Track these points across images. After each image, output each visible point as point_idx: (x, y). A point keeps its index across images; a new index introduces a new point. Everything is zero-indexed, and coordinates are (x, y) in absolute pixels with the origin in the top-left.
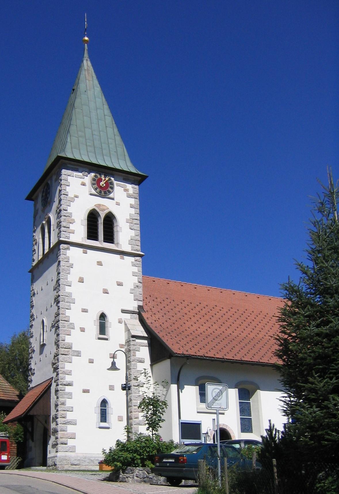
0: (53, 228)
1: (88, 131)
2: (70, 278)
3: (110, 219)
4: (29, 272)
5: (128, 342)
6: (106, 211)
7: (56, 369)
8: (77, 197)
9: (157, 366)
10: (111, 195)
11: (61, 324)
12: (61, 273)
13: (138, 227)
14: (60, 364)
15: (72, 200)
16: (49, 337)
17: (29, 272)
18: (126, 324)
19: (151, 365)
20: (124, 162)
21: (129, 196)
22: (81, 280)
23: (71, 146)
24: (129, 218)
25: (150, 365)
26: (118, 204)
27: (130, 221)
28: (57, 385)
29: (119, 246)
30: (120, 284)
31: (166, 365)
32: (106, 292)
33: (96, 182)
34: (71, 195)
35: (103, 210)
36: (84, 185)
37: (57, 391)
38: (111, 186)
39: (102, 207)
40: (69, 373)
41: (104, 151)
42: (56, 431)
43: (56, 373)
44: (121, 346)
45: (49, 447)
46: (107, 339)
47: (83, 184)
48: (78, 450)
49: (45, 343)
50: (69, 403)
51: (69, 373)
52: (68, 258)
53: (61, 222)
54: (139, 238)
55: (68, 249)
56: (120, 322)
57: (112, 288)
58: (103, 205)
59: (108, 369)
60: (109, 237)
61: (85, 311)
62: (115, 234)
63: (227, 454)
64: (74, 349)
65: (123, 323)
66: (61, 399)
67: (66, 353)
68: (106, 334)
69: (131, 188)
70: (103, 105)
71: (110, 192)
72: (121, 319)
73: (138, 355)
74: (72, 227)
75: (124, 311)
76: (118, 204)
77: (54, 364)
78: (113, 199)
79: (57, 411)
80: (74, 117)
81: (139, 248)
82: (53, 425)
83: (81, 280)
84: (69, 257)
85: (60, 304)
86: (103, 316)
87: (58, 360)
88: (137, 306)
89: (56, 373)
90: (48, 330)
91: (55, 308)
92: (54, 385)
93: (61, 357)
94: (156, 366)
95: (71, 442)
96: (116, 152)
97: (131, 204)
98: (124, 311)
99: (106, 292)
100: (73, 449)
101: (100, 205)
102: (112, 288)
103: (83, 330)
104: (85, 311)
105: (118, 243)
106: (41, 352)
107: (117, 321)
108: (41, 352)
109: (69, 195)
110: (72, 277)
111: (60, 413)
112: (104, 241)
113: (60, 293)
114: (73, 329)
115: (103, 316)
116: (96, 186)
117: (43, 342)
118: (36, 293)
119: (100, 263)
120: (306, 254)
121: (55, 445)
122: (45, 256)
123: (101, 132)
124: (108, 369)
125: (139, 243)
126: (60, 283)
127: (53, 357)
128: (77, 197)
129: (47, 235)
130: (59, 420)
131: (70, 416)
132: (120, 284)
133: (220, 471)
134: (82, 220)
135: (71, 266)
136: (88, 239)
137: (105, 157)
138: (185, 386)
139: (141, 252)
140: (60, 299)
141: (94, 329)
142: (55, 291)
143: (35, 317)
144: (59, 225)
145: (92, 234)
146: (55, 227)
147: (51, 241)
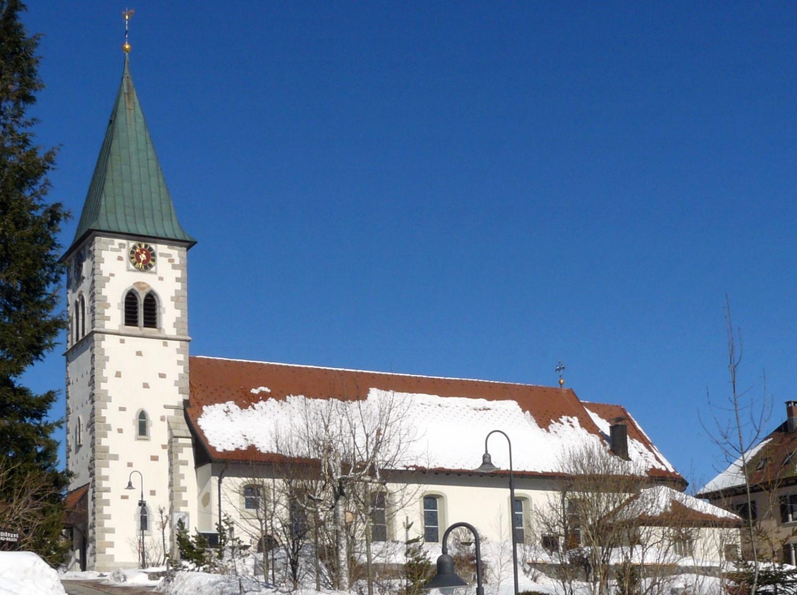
0: (88, 310)
1: (127, 185)
2: (105, 373)
3: (151, 301)
4: (64, 355)
5: (170, 442)
6: (147, 291)
7: (92, 474)
8: (112, 275)
10: (153, 269)
11: (96, 425)
13: (185, 305)
14: (96, 470)
16: (85, 437)
17: (64, 355)
18: (168, 423)
20: (170, 222)
21: (174, 267)
22: (118, 375)
25: (195, 468)
26: (161, 279)
27: (176, 299)
29: (162, 331)
30: (162, 376)
31: (208, 467)
32: (146, 386)
33: (134, 255)
34: (105, 274)
35: (143, 289)
36: (120, 260)
37: (93, 498)
38: (153, 258)
40: (106, 478)
41: (146, 212)
42: (93, 540)
43: (92, 478)
44: (164, 447)
45: (88, 556)
47: (120, 258)
49: (81, 443)
51: (106, 478)
52: (103, 350)
55: (103, 339)
56: (162, 419)
57: (154, 381)
58: (144, 283)
59: (126, 489)
60: (151, 320)
61: (122, 409)
62: (158, 316)
63: (348, 560)
64: (111, 452)
65: (166, 421)
66: (97, 507)
67: (102, 458)
70: (147, 143)
71: (151, 266)
73: (181, 457)
75: (165, 407)
76: (161, 279)
77: (90, 469)
78: (155, 273)
79: (94, 519)
80: (109, 168)
81: (186, 331)
82: (90, 532)
83: (118, 375)
85: (96, 403)
86: (142, 415)
87: (94, 465)
88: (181, 400)
89: (92, 478)
90: (84, 429)
93: (97, 462)
96: (161, 211)
99: (146, 386)
100: (112, 557)
101: (139, 283)
102: (154, 381)
103: (120, 431)
104: (122, 409)
105: (160, 328)
106: (77, 452)
108: (77, 452)
110: (108, 371)
111: (98, 520)
112: (145, 326)
114: (110, 430)
115: (142, 415)
117: (79, 442)
118: (71, 382)
119: (139, 353)
121: (93, 554)
124: (126, 489)
127: (89, 461)
128: (112, 275)
130: (96, 529)
131: (107, 524)
132: (162, 376)
133: (157, 568)
134: (119, 304)
135: (107, 359)
136: (126, 325)
139: (188, 335)
140: (96, 398)
141: (132, 429)
143: (71, 411)
144: (93, 309)
145: (130, 319)
146: (89, 311)
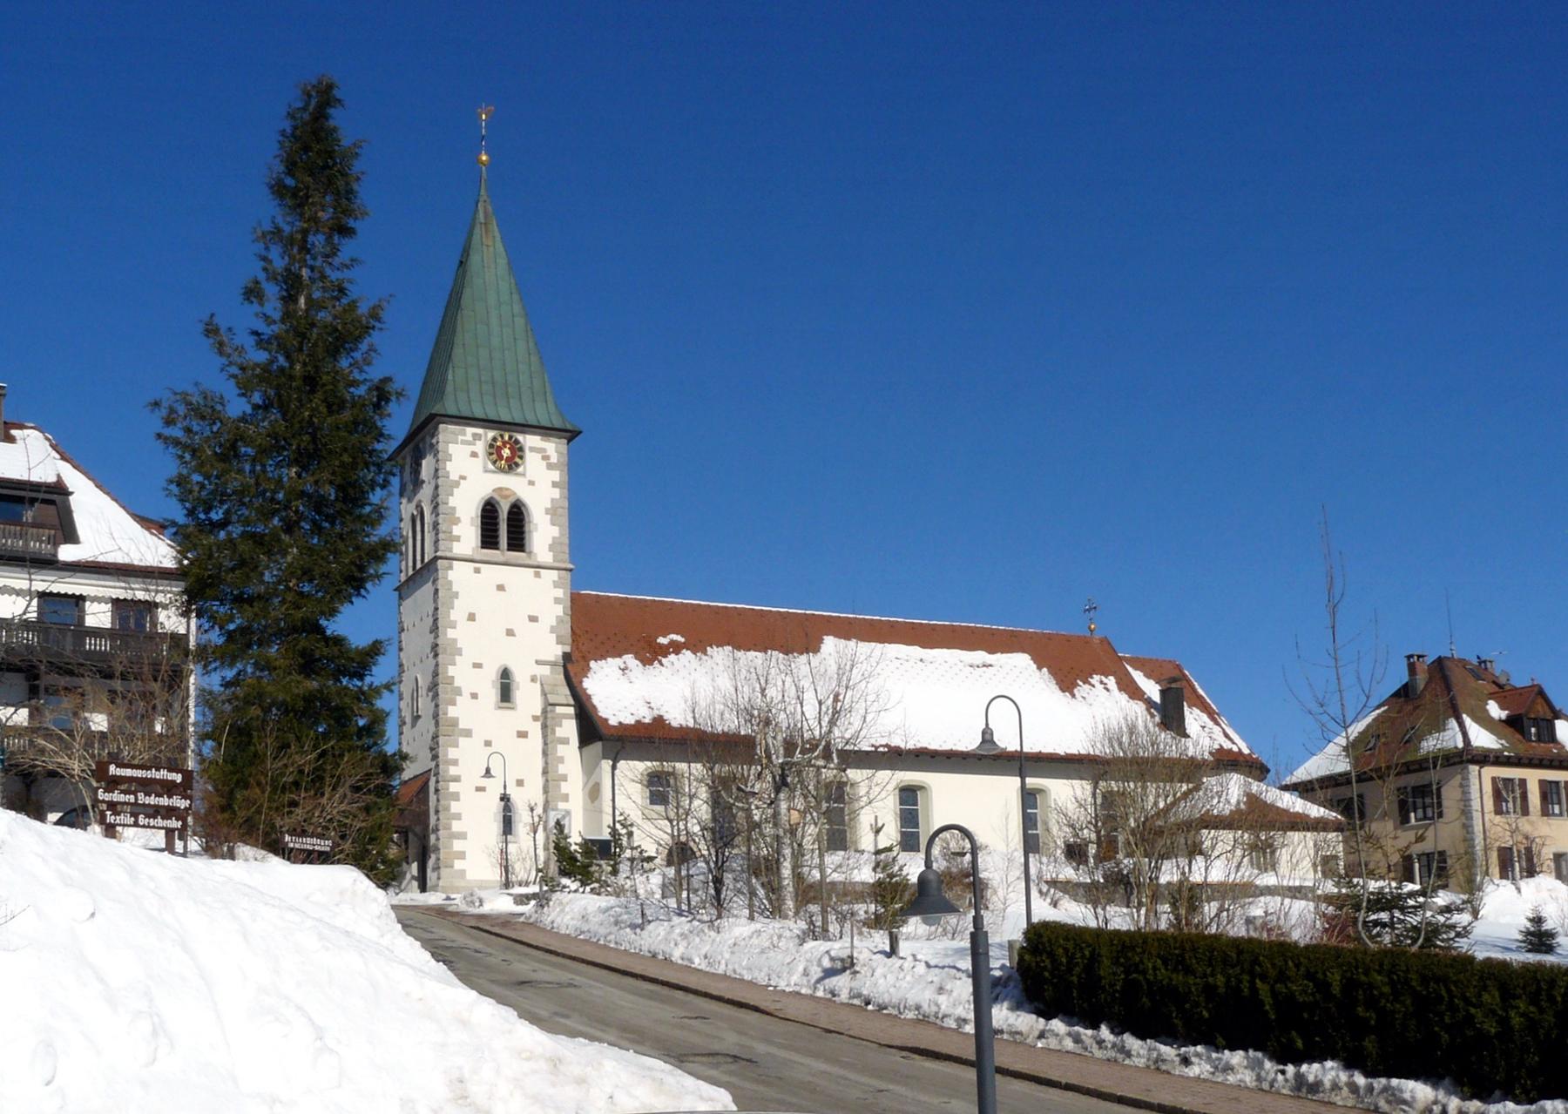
2: (454, 615)
3: (518, 514)
4: (395, 590)
5: (544, 711)
6: (512, 499)
7: (435, 757)
9: (587, 749)
10: (520, 470)
13: (565, 520)
15: (457, 484)
16: (425, 704)
17: (395, 590)
18: (542, 685)
19: (581, 747)
21: (550, 467)
22: (472, 617)
26: (531, 483)
27: (552, 512)
28: (437, 782)
30: (533, 619)
32: (510, 633)
33: (494, 450)
34: (454, 476)
35: (506, 497)
37: (437, 790)
38: (520, 453)
40: (455, 762)
41: (510, 389)
42: (437, 849)
43: (434, 763)
44: (535, 718)
46: (513, 708)
47: (474, 455)
50: (455, 807)
51: (455, 762)
52: (451, 582)
54: (567, 541)
55: (451, 568)
56: (533, 679)
57: (522, 626)
58: (507, 489)
60: (518, 541)
61: (477, 666)
68: (527, 550)
71: (517, 465)
72: (535, 676)
74: (456, 530)
76: (531, 483)
79: (438, 819)
83: (472, 617)
86: (505, 674)
87: (438, 743)
88: (561, 654)
89: (434, 763)
90: (424, 693)
91: (431, 662)
92: (433, 779)
93: (441, 740)
96: (531, 388)
98: (537, 662)
99: (510, 633)
100: (462, 873)
101: (500, 489)
102: (522, 626)
103: (474, 696)
104: (477, 666)
105: (530, 553)
107: (529, 679)
108: (413, 726)
109: (451, 478)
110: (457, 613)
112: (509, 550)
113: (439, 641)
114: (461, 695)
115: (505, 674)
116: (494, 457)
119: (501, 588)
120: (991, 907)
121: (437, 868)
122: (417, 573)
123: (506, 352)
125: (567, 550)
129: (418, 528)
130: (441, 833)
131: (456, 826)
132: (533, 619)
134: (472, 518)
135: (456, 595)
136: (482, 547)
137: (511, 400)
140: (440, 650)
141: (491, 693)
142: (433, 635)
144: (436, 525)
145: (489, 539)
147: (426, 551)
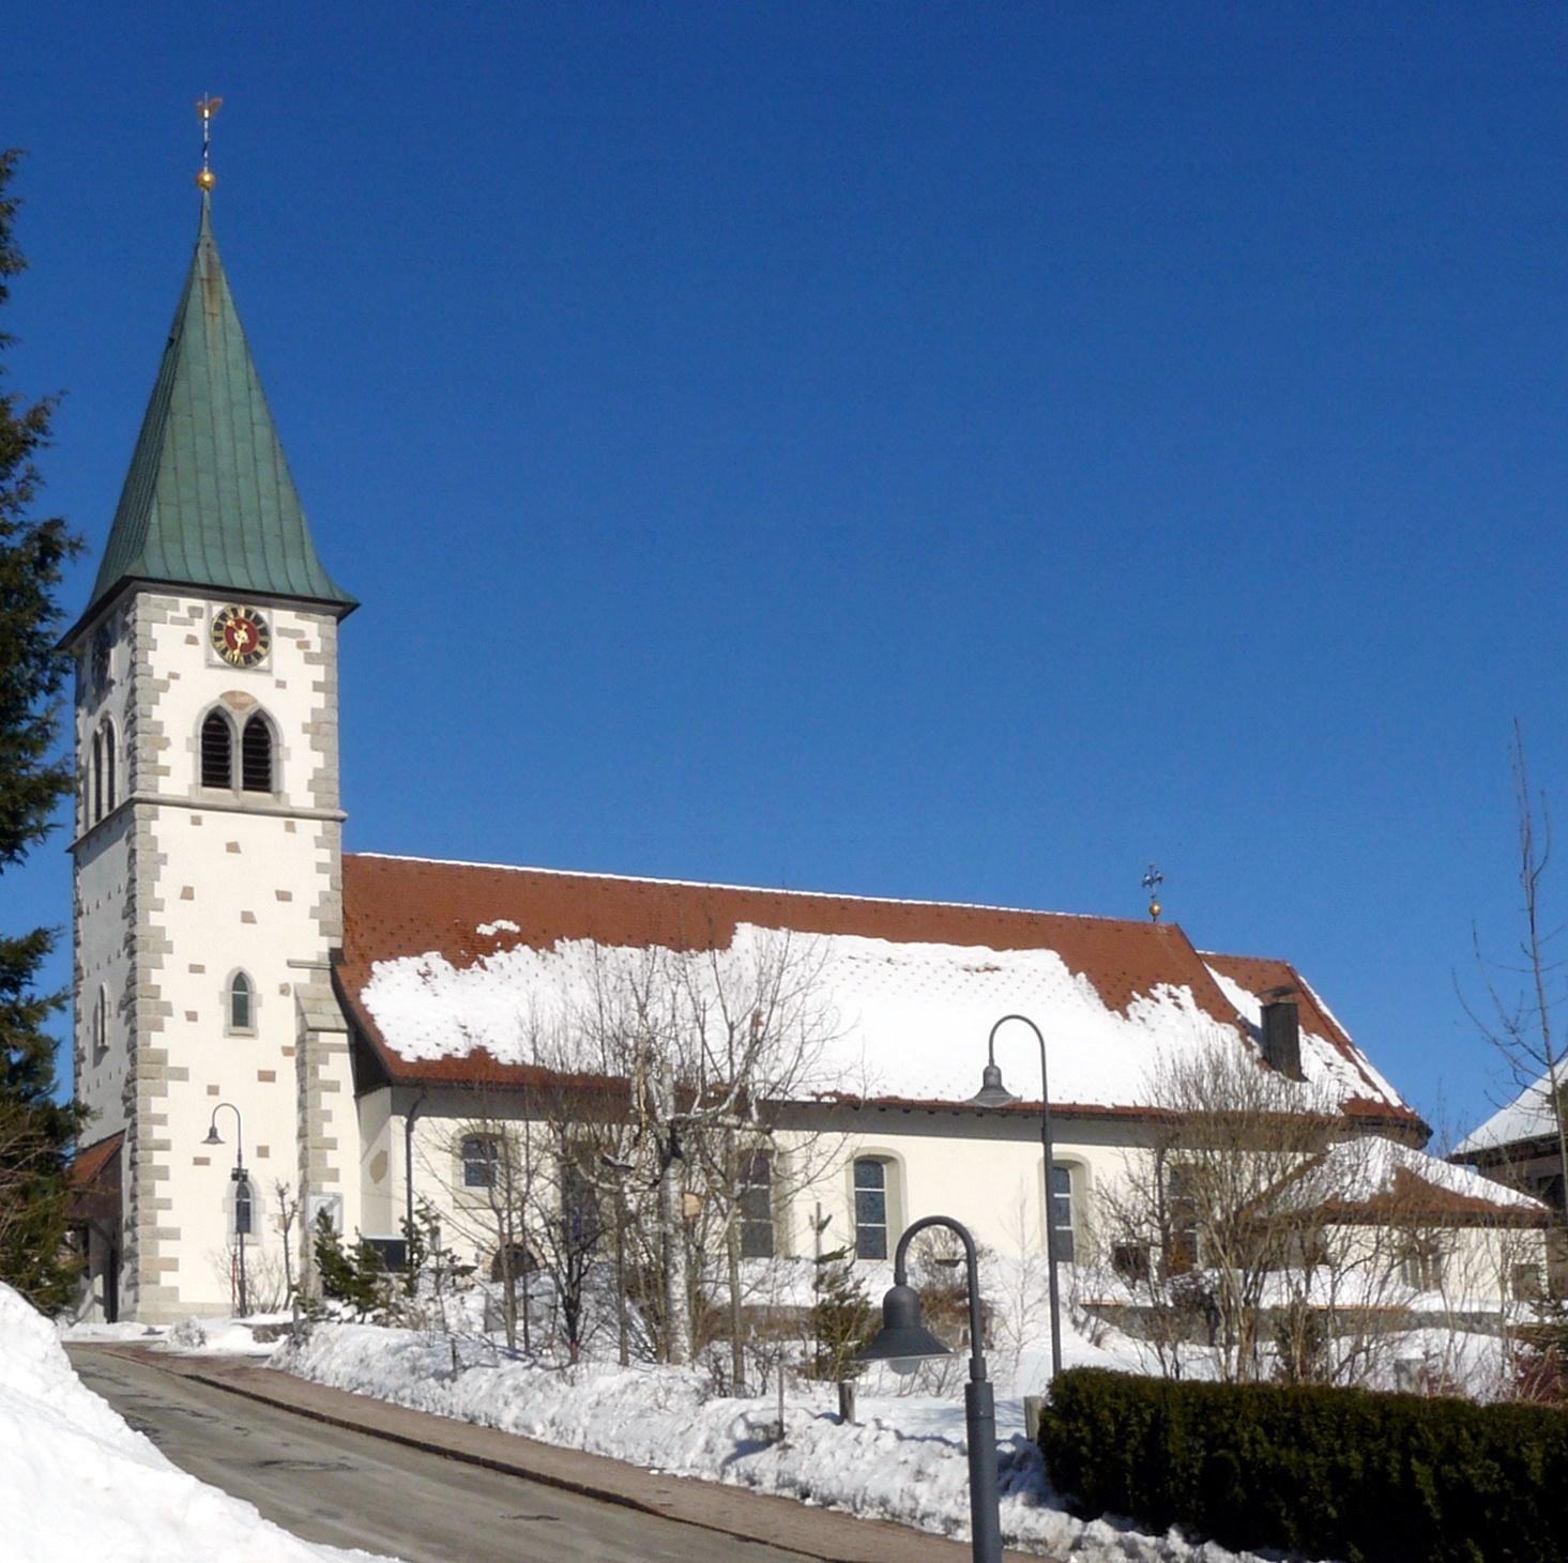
1: (206, 481)
2: (160, 891)
3: (259, 733)
4: (69, 851)
5: (301, 1041)
6: (250, 710)
7: (131, 1112)
8: (174, 676)
10: (263, 663)
11: (140, 1004)
12: (139, 881)
13: (333, 743)
14: (140, 1102)
15: (165, 686)
16: (115, 1030)
17: (69, 851)
19: (357, 1097)
21: (310, 659)
22: (188, 894)
23: (91, 1437)
24: (309, 720)
26: (281, 684)
27: (313, 729)
29: (283, 799)
30: (284, 896)
31: (383, 1096)
32: (248, 918)
33: (222, 634)
34: (160, 674)
35: (241, 706)
36: (192, 643)
37: (133, 1164)
38: (263, 638)
39: (240, 700)
40: (162, 1120)
42: (133, 1255)
44: (287, 1051)
46: (251, 1036)
47: (192, 640)
48: (183, 1298)
49: (106, 1043)
51: (162, 1120)
53: (135, 748)
56: (284, 990)
57: (266, 906)
58: (243, 694)
60: (260, 774)
61: (197, 969)
62: (273, 766)
64: (171, 1063)
65: (292, 995)
69: (315, 629)
71: (259, 656)
73: (325, 1073)
74: (164, 758)
75: (291, 964)
76: (281, 684)
77: (125, 1099)
78: (269, 671)
79: (135, 1209)
81: (335, 799)
83: (188, 894)
84: (155, 838)
86: (240, 982)
87: (134, 1090)
88: (326, 950)
92: (127, 1147)
93: (140, 1084)
94: (365, 1099)
95: (167, 1279)
96: (281, 536)
97: (315, 683)
99: (248, 918)
101: (232, 694)
102: (266, 906)
103: (192, 1016)
104: (197, 969)
105: (279, 793)
106: (97, 1062)
107: (277, 991)
108: (97, 1062)
109: (156, 676)
110: (165, 887)
111: (143, 1211)
112: (245, 788)
113: (137, 931)
115: (240, 982)
117: (103, 1041)
118: (85, 910)
119: (233, 848)
121: (133, 1285)
122: (102, 824)
126: (137, 906)
128: (174, 676)
129: (105, 755)
131: (164, 1219)
132: (284, 896)
134: (188, 739)
135: (163, 859)
136: (204, 785)
138: (739, 925)
139: (341, 808)
140: (138, 944)
141: (218, 1013)
142: (127, 921)
143: (85, 974)
144: (131, 750)
145: (214, 771)
147: (116, 790)
